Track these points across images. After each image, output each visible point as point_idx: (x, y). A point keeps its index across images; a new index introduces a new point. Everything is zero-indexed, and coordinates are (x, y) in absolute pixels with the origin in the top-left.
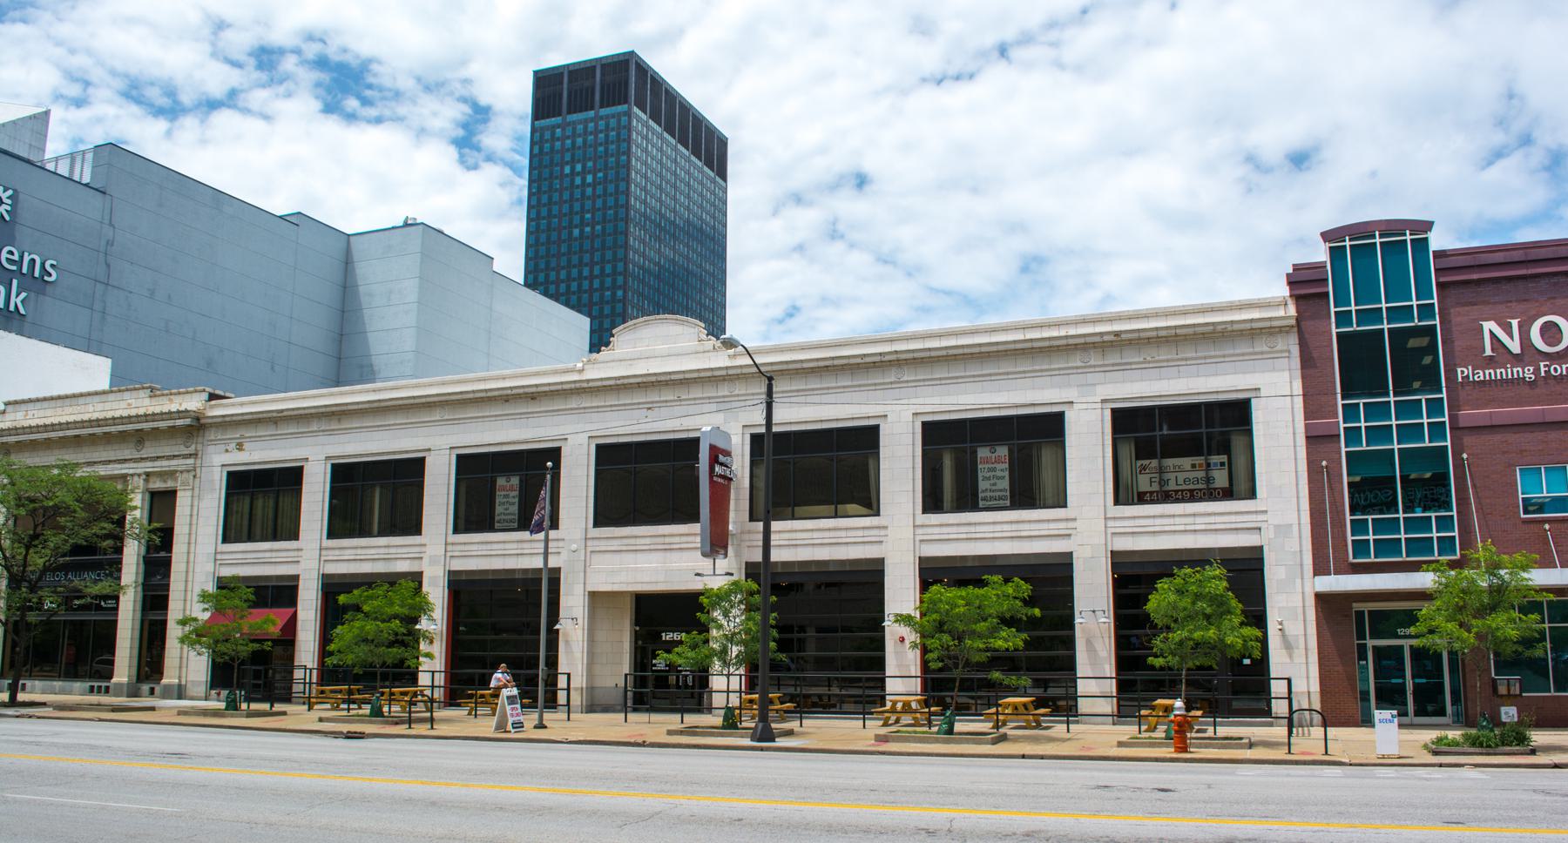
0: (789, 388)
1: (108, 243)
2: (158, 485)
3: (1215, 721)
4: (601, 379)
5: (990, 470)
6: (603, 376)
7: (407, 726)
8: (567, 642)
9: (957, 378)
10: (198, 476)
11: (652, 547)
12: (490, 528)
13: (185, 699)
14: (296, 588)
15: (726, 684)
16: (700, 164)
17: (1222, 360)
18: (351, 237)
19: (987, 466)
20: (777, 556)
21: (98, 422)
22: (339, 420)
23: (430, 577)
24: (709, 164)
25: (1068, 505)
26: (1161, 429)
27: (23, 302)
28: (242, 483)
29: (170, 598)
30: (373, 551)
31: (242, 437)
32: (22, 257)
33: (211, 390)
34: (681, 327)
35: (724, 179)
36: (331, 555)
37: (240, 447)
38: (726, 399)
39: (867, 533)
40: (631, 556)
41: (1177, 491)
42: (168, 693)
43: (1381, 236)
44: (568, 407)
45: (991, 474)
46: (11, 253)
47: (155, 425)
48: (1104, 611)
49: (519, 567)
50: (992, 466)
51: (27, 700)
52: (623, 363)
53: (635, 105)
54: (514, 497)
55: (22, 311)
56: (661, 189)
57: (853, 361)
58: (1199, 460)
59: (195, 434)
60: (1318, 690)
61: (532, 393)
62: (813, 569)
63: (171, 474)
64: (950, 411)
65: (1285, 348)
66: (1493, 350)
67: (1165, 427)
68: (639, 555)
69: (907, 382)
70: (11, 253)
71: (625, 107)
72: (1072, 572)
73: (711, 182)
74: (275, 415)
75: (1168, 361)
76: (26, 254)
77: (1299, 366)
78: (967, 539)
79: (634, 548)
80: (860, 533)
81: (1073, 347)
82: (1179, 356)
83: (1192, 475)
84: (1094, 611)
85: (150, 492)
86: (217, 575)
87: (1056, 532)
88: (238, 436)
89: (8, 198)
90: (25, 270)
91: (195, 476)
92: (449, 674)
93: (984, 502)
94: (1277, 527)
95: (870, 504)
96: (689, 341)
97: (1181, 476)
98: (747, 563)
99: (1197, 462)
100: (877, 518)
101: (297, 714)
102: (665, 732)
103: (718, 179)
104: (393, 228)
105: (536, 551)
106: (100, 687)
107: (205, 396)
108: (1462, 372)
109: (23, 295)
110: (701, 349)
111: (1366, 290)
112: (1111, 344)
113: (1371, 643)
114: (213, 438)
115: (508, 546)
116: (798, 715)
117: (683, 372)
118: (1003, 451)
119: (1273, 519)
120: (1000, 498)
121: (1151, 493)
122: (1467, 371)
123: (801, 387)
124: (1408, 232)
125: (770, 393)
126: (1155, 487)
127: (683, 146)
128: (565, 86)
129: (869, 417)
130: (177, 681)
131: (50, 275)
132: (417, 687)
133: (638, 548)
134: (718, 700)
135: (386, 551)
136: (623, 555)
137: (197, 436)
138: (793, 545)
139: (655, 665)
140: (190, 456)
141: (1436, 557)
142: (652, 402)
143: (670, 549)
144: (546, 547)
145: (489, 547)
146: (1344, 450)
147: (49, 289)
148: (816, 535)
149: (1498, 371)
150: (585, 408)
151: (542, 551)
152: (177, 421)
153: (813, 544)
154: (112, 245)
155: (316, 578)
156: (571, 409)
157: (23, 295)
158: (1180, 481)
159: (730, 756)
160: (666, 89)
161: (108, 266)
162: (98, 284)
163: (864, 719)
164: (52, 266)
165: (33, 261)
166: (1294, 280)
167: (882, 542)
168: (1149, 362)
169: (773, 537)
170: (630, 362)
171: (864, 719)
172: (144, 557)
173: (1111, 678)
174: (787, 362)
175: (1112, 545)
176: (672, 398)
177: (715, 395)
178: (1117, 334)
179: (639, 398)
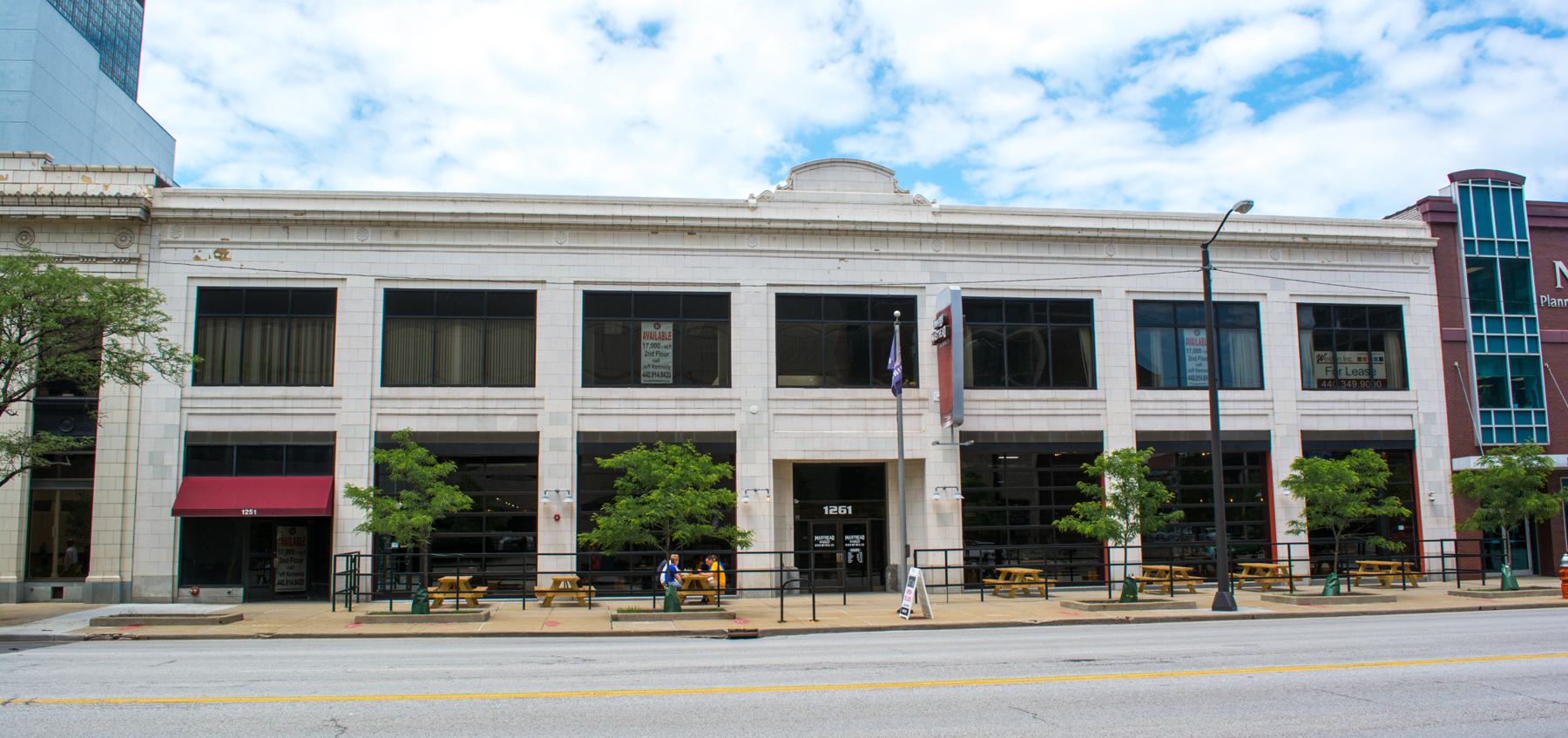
0: (999, 254)
3: (1348, 580)
4: (787, 221)
5: (653, 345)
9: (1166, 261)
11: (851, 412)
12: (637, 383)
13: (131, 602)
15: (1125, 557)
19: (650, 342)
20: (1226, 425)
22: (396, 234)
23: (551, 439)
26: (1336, 326)
29: (97, 459)
30: (459, 404)
31: (224, 241)
36: (389, 407)
37: (222, 254)
38: (932, 258)
39: (1085, 405)
41: (1347, 381)
42: (101, 594)
43: (1473, 182)
45: (1197, 355)
47: (70, 211)
48: (768, 490)
49: (678, 429)
50: (1198, 347)
52: (807, 205)
54: (666, 347)
57: (1070, 233)
58: (1363, 354)
61: (692, 227)
62: (1032, 440)
64: (287, 279)
66: (1562, 283)
67: (1338, 324)
68: (834, 419)
69: (1120, 259)
74: (289, 216)
75: (1341, 266)
78: (1179, 415)
79: (829, 412)
80: (1078, 405)
81: (220, 221)
83: (1358, 367)
84: (557, 491)
86: (184, 429)
87: (1248, 412)
88: (219, 240)
92: (1272, 542)
93: (646, 379)
94: (1426, 415)
95: (324, 376)
96: (885, 191)
97: (1351, 368)
99: (1362, 356)
100: (532, 388)
101: (1433, 591)
105: (887, 412)
108: (1544, 299)
110: (899, 200)
112: (1297, 245)
114: (170, 239)
116: (979, 590)
117: (888, 224)
118: (667, 328)
119: (549, 406)
120: (663, 375)
121: (1327, 381)
122: (1547, 298)
123: (1138, 257)
124: (1509, 183)
125: (1206, 261)
126: (1330, 376)
129: (1082, 291)
130: (118, 577)
132: (1276, 561)
133: (834, 412)
134: (1117, 573)
135: (481, 404)
138: (1009, 415)
139: (818, 542)
140: (129, 260)
141: (1515, 443)
142: (846, 253)
144: (900, 408)
145: (636, 404)
148: (1034, 405)
149: (1559, 300)
150: (761, 251)
151: (895, 412)
152: (113, 209)
153: (1031, 415)
155: (368, 436)
156: (353, 245)
158: (1350, 372)
159: (560, 642)
163: (982, 593)
167: (334, 414)
168: (1327, 265)
169: (1220, 405)
170: (814, 205)
171: (982, 593)
173: (366, 556)
175: (578, 426)
177: (919, 252)
178: (1305, 237)
179: (829, 246)
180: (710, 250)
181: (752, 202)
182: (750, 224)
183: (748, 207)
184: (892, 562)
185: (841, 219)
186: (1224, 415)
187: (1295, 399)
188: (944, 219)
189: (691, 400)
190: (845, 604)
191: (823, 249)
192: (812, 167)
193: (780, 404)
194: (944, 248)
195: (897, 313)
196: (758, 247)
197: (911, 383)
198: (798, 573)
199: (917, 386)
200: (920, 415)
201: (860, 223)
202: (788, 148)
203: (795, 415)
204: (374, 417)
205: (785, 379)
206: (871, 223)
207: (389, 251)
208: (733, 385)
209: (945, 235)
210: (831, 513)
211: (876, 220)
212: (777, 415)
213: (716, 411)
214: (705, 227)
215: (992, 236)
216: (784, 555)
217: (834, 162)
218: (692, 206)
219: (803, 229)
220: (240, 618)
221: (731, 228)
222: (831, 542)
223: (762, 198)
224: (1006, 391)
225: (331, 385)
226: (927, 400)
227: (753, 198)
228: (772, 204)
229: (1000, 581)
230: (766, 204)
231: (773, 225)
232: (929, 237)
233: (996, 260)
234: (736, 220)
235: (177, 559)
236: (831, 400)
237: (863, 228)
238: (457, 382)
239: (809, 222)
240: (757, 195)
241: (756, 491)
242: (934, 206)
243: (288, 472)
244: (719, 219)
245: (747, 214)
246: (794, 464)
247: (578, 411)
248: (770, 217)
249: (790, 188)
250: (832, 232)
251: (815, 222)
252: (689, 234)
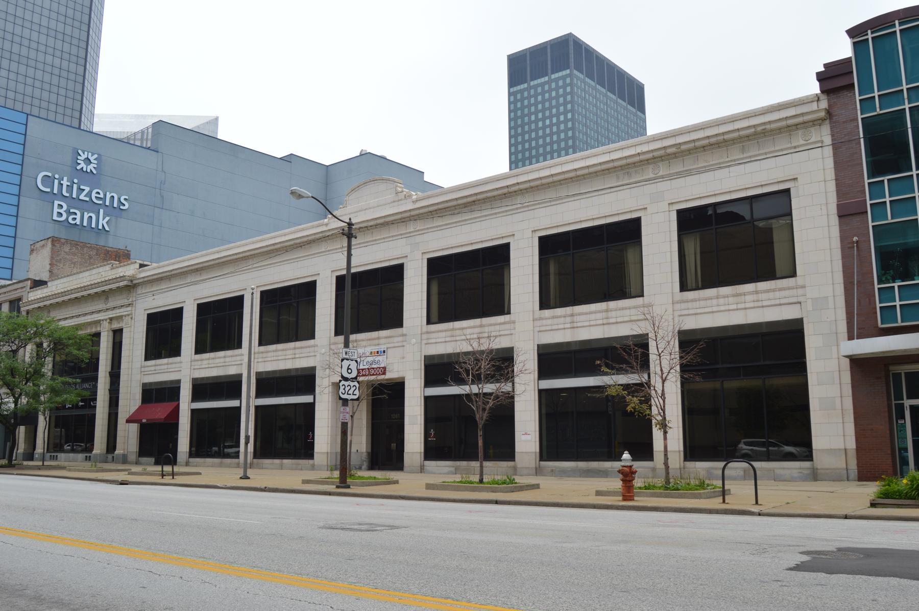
1: (161, 183)
2: (116, 326)
7: (171, 477)
10: (133, 318)
14: (179, 388)
16: (624, 104)
17: (765, 157)
18: (328, 167)
21: (92, 286)
24: (631, 103)
25: (645, 294)
27: (107, 223)
28: (154, 320)
32: (105, 195)
33: (142, 262)
35: (643, 112)
36: (197, 365)
38: (412, 234)
46: (98, 193)
53: (575, 69)
55: (107, 228)
56: (597, 124)
59: (132, 291)
60: (854, 447)
63: (119, 318)
65: (819, 139)
70: (98, 193)
71: (568, 71)
73: (634, 116)
76: (108, 193)
77: (831, 154)
82: (729, 159)
85: (112, 331)
89: (95, 159)
90: (107, 203)
91: (132, 318)
98: (425, 356)
102: (301, 482)
103: (639, 113)
104: (356, 157)
106: (54, 456)
107: (137, 266)
109: (107, 218)
111: (888, 76)
112: (675, 156)
113: (908, 403)
114: (140, 293)
127: (611, 93)
128: (528, 62)
131: (124, 205)
133: (699, 311)
137: (133, 292)
146: (871, 224)
147: (124, 213)
154: (164, 184)
155: (189, 381)
157: (107, 218)
160: (596, 56)
161: (162, 197)
162: (156, 209)
164: (125, 199)
165: (113, 197)
166: (822, 78)
172: (109, 372)
174: (447, 201)
180: (280, 262)
187: (516, 324)
194: (418, 227)
204: (192, 371)
207: (623, 190)
220: (537, 486)
225: (509, 313)
235: (138, 444)
238: (694, 287)
243: (168, 401)
247: (538, 329)
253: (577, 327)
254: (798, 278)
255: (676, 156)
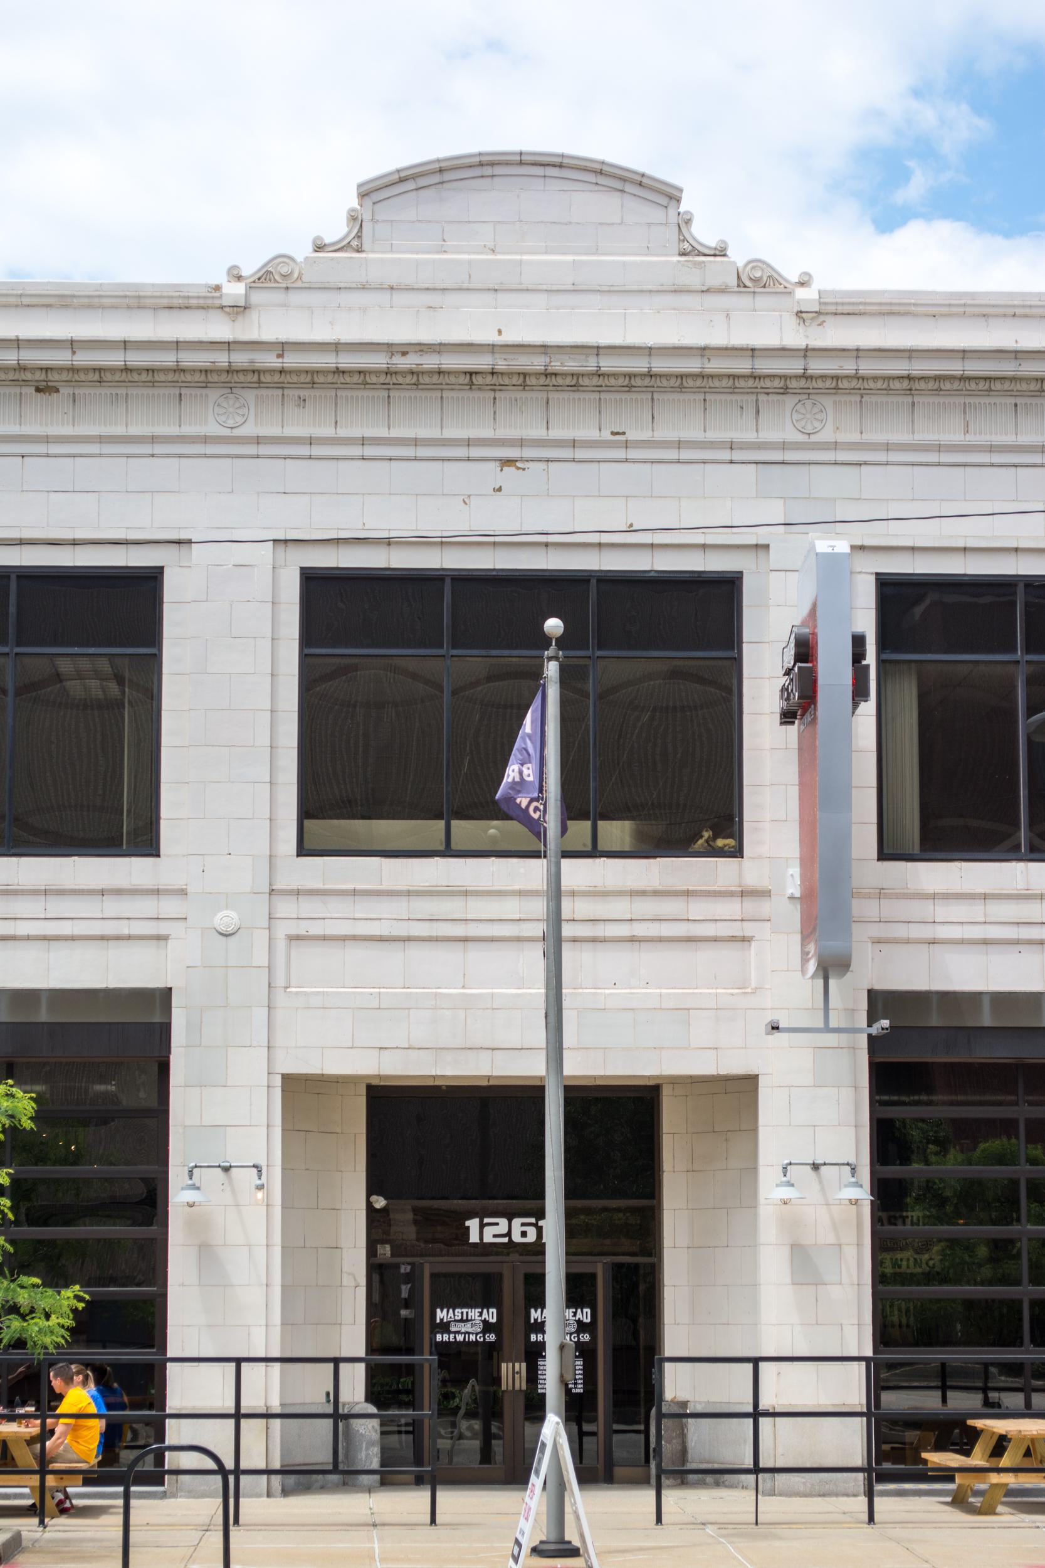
0: (1009, 439)
4: (337, 347)
6: (718, 339)
8: (206, 1251)
34: (615, 199)
38: (790, 456)
40: (448, 958)
44: (188, 430)
51: (917, 1498)
52: (400, 298)
68: (476, 955)
72: (169, 1051)
81: (303, 378)
96: (648, 251)
110: (693, 279)
115: (698, 909)
116: (121, 1489)
117: (650, 351)
133: (472, 930)
136: (415, 952)
139: (445, 1327)
142: (521, 443)
143: (594, 940)
144: (555, 919)
150: (258, 440)
151: (537, 929)
156: (205, 440)
176: (593, 434)
177: (750, 436)
180: (101, 439)
181: (235, 291)
182: (221, 359)
183: (222, 307)
184: (669, 1395)
185: (510, 337)
186: (575, 940)
188: (836, 335)
189: (35, 892)
190: (433, 1521)
191: (450, 433)
192: (422, 182)
193: (308, 907)
194: (830, 426)
195: (553, 625)
196: (249, 429)
197: (720, 842)
198: (375, 1423)
199: (737, 852)
200: (745, 940)
201: (613, 349)
202: (927, 116)
203: (354, 938)
205: (321, 828)
206: (598, 350)
208: (300, 858)
209: (835, 384)
210: (488, 1238)
211: (617, 340)
212: (298, 938)
213: (109, 928)
214: (86, 370)
215: (982, 385)
216: (763, 1365)
217: (492, 164)
218: (49, 306)
219: (388, 372)
221: (165, 370)
222: (487, 1327)
223: (265, 278)
224: (1020, 866)
226: (764, 894)
227: (239, 278)
228: (295, 298)
229: (977, 1459)
230: (278, 297)
231: (292, 360)
232: (785, 391)
233: (997, 458)
234: (178, 345)
236: (466, 893)
237: (571, 364)
239: (404, 349)
240: (249, 269)
241: (227, 1169)
242: (801, 293)
244: (126, 345)
245: (219, 329)
246: (370, 1088)
248: (283, 337)
249: (354, 243)
250: (478, 380)
251: (422, 348)
252: (38, 390)
253: (908, 941)
254: (746, 862)
255: (471, 384)
